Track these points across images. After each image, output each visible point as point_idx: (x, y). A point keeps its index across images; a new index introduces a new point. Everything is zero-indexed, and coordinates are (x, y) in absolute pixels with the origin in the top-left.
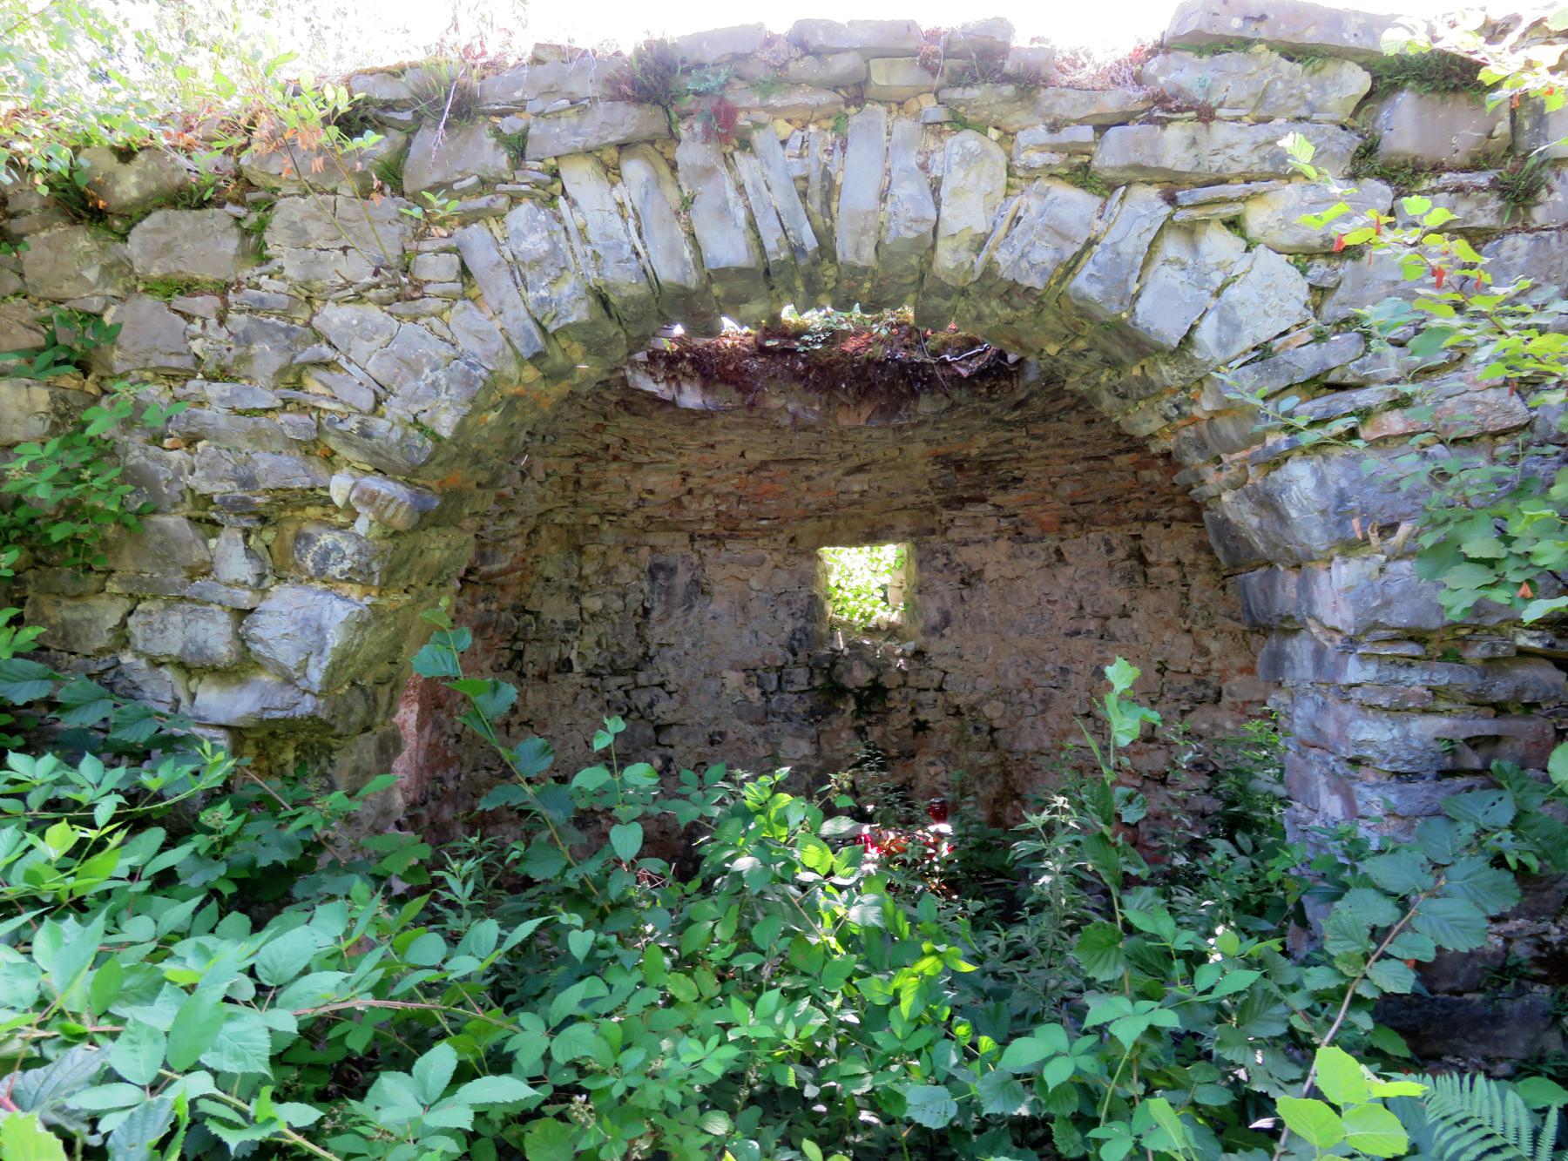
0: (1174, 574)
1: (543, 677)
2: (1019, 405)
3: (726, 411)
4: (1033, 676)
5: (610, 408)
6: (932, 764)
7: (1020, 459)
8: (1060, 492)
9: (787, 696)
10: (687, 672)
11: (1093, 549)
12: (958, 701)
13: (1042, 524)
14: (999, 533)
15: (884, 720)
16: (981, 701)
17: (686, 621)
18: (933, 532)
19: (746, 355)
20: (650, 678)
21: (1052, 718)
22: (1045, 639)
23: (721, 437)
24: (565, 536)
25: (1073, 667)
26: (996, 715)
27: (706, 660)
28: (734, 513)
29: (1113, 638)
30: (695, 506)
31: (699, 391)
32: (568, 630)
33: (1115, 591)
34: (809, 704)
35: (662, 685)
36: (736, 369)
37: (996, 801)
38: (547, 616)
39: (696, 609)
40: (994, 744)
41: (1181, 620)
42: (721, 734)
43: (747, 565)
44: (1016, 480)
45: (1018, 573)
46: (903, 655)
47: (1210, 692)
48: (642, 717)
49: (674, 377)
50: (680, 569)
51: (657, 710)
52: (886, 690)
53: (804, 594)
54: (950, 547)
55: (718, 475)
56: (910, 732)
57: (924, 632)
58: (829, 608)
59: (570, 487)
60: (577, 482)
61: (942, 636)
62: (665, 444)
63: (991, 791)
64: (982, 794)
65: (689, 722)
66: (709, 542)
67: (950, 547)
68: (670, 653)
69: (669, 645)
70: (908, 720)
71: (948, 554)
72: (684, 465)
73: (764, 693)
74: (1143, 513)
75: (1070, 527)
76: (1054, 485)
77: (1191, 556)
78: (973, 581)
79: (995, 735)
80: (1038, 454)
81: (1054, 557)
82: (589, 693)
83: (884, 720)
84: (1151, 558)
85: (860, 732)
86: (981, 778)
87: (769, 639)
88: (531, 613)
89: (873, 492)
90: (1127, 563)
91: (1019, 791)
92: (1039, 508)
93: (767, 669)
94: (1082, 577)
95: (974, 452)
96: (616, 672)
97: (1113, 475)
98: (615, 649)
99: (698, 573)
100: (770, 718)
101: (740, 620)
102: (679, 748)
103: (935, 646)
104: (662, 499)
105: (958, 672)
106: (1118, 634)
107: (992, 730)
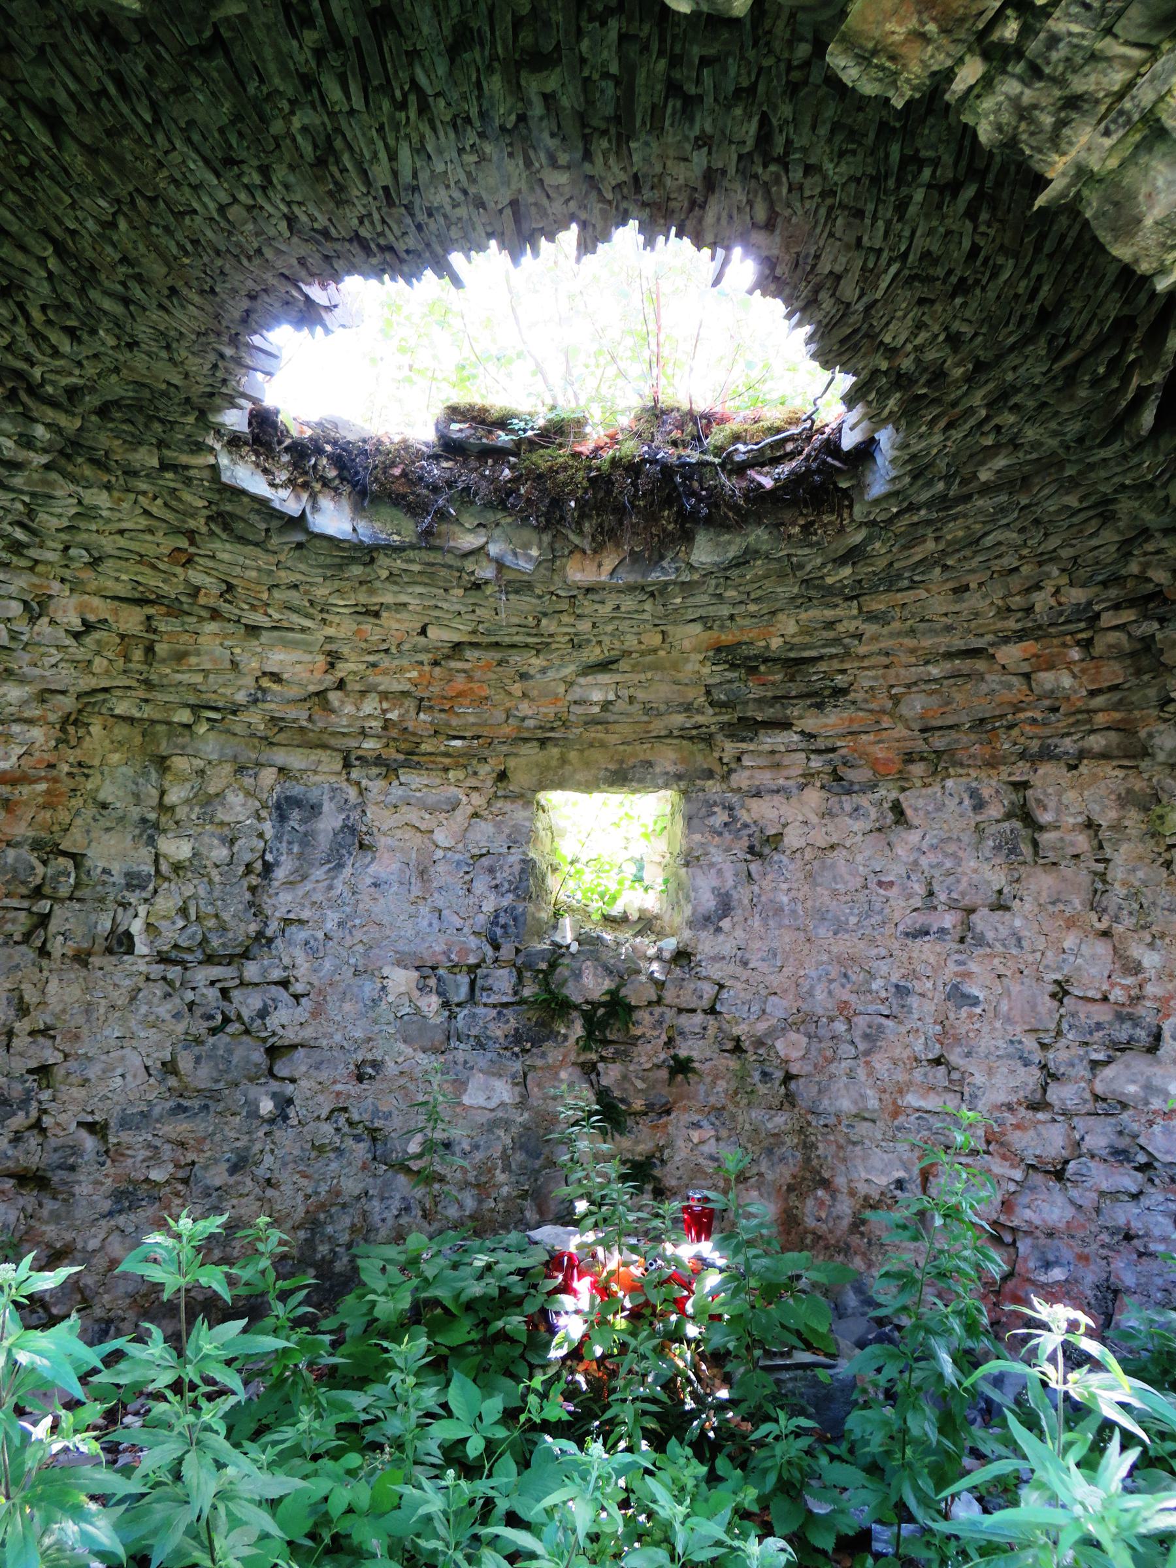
0: (1082, 842)
1: (81, 959)
2: (852, 555)
3: (398, 549)
4: (853, 998)
5: (198, 524)
6: (696, 1125)
7: (847, 654)
8: (904, 710)
9: (480, 1010)
10: (328, 965)
11: (951, 804)
12: (737, 1031)
13: (874, 764)
14: (808, 776)
15: (626, 1053)
16: (771, 1032)
17: (330, 887)
18: (710, 774)
19: (420, 455)
20: (264, 971)
21: (880, 1063)
22: (872, 941)
23: (388, 599)
24: (138, 740)
25: (918, 986)
26: (795, 1054)
27: (360, 948)
28: (410, 725)
29: (981, 941)
30: (349, 709)
31: (346, 505)
32: (130, 887)
33: (986, 867)
34: (513, 1023)
35: (285, 984)
36: (404, 474)
37: (791, 1188)
38: (97, 859)
39: (348, 871)
40: (790, 1099)
41: (1094, 916)
42: (375, 1064)
43: (431, 810)
44: (839, 692)
45: (834, 839)
46: (658, 958)
47: (1141, 1034)
48: (247, 1032)
49: (306, 486)
50: (327, 807)
51: (273, 1021)
52: (630, 1009)
53: (514, 858)
54: (734, 799)
55: (386, 662)
56: (664, 1074)
57: (691, 924)
58: (552, 882)
59: (138, 654)
60: (150, 650)
61: (719, 930)
62: (294, 597)
63: (783, 1173)
64: (769, 1177)
65: (324, 1043)
66: (375, 771)
67: (734, 799)
68: (302, 935)
69: (301, 922)
70: (662, 1056)
71: (731, 809)
72: (329, 639)
73: (446, 1004)
74: (1035, 746)
75: (918, 769)
76: (896, 700)
77: (1113, 814)
78: (766, 851)
79: (793, 1085)
80: (874, 648)
81: (890, 817)
82: (159, 989)
83: (626, 1053)
84: (1045, 818)
85: (589, 1070)
86: (770, 1151)
87: (458, 923)
88: (65, 854)
89: (620, 706)
90: (1006, 825)
91: (826, 1175)
92: (871, 737)
93: (454, 968)
94: (934, 847)
95: (776, 643)
96: (210, 959)
97: (993, 679)
98: (211, 923)
99: (355, 815)
100: (454, 1043)
101: (416, 891)
102: (304, 1083)
103: (706, 945)
104: (294, 692)
105: (739, 985)
106: (990, 935)
107: (789, 1078)
